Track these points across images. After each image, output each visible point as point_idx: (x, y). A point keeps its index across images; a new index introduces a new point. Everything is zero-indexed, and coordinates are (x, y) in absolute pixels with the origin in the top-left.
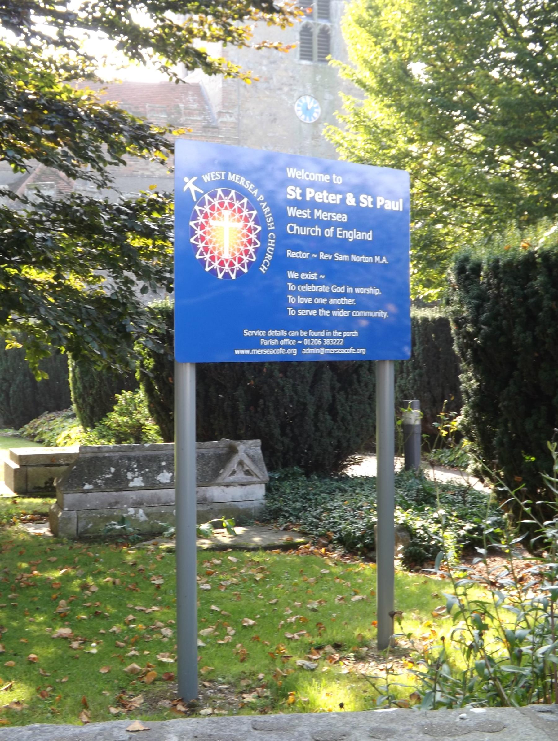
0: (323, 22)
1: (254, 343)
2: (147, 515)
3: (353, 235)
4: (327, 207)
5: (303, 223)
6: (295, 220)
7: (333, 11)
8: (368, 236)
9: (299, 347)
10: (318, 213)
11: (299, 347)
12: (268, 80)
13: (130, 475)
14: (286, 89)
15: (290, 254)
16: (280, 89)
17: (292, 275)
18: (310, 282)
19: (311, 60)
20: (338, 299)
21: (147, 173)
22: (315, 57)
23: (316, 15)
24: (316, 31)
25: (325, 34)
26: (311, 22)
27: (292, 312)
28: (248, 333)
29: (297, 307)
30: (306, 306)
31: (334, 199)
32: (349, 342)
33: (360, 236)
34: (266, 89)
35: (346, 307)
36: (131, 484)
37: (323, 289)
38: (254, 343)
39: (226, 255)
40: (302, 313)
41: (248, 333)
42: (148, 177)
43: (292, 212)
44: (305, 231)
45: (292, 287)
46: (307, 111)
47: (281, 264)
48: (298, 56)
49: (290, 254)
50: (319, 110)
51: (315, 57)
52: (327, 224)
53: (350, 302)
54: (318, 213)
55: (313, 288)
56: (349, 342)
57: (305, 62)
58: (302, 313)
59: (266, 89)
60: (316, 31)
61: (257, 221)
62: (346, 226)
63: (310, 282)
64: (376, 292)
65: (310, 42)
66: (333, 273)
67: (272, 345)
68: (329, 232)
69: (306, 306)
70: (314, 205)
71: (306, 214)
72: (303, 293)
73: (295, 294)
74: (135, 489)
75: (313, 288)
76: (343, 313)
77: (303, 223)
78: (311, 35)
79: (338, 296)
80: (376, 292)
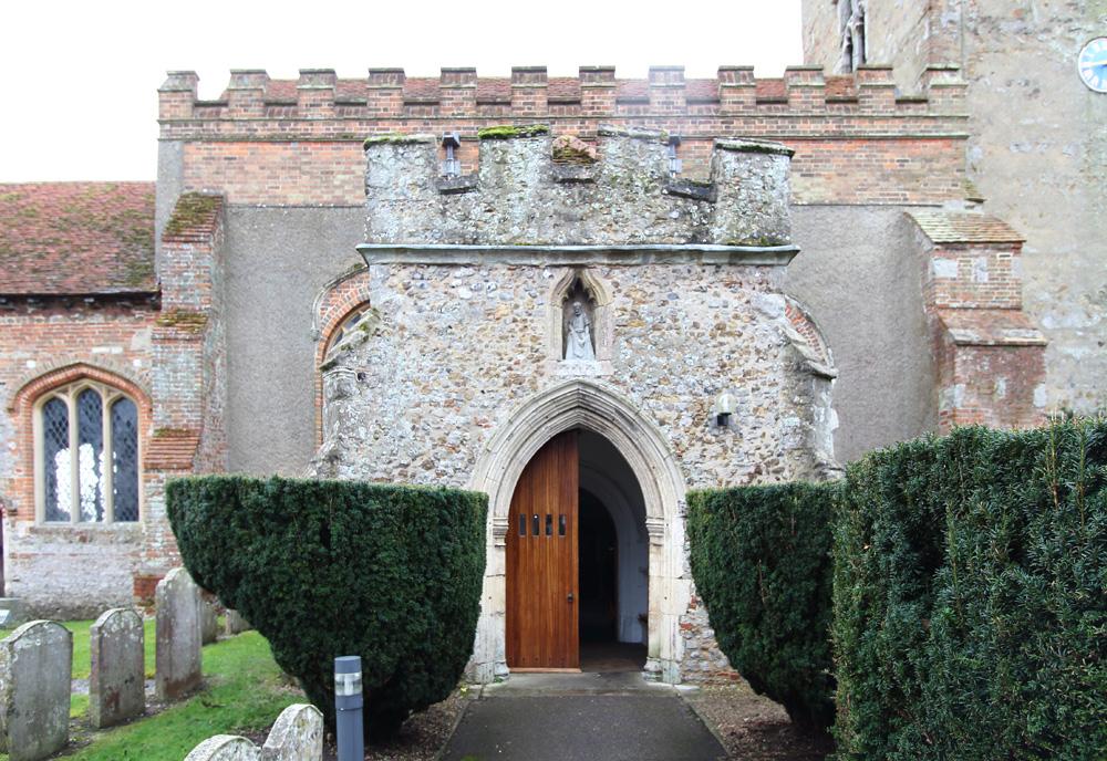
14: (1058, 30)
16: (1047, 30)
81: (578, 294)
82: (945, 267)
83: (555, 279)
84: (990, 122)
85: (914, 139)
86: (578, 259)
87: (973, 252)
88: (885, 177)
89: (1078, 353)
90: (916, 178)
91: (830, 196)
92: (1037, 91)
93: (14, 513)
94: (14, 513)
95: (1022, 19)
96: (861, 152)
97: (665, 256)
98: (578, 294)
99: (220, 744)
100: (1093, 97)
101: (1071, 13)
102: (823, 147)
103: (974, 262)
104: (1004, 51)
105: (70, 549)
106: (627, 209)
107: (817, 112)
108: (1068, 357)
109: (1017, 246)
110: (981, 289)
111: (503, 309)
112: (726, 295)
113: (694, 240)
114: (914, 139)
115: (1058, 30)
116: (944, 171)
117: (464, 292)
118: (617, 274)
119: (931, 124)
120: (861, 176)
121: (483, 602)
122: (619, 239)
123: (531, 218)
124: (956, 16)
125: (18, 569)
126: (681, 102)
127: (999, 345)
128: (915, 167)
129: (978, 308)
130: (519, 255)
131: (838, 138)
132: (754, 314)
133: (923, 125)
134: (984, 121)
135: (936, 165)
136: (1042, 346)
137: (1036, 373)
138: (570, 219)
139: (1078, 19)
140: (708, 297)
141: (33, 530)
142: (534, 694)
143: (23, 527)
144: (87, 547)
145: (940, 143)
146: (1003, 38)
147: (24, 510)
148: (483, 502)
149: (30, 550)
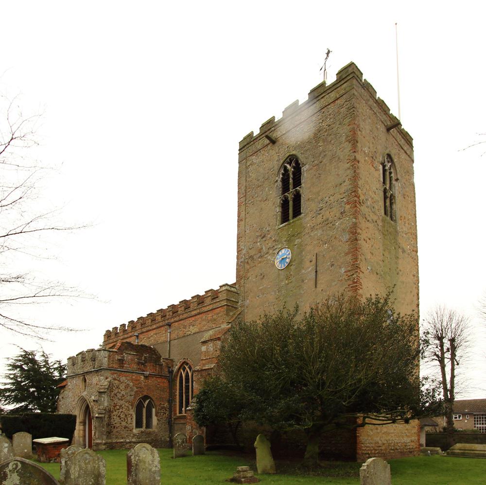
14: (271, 251)
84: (251, 292)
85: (214, 309)
87: (210, 343)
90: (215, 320)
91: (198, 330)
92: (264, 276)
95: (260, 252)
96: (204, 316)
99: (468, 343)
100: (280, 272)
102: (196, 317)
103: (209, 345)
104: (255, 266)
107: (195, 308)
114: (214, 309)
119: (218, 303)
120: (204, 323)
121: (76, 428)
126: (171, 314)
128: (215, 317)
129: (209, 358)
131: (199, 314)
133: (217, 304)
134: (249, 292)
135: (220, 315)
139: (276, 245)
145: (220, 309)
146: (255, 261)
148: (75, 417)
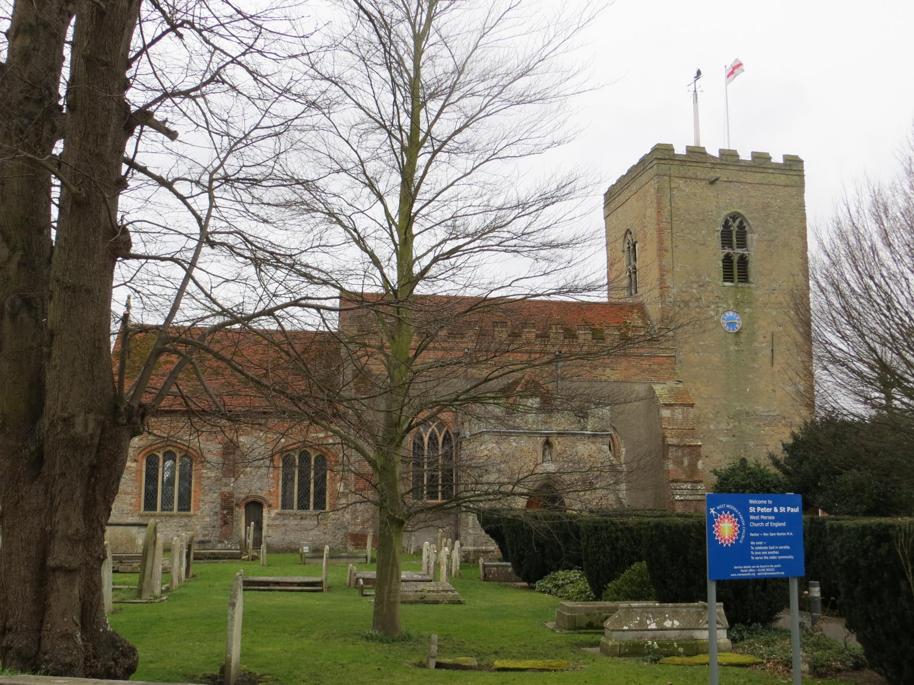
0: (740, 251)
1: (738, 571)
2: (659, 645)
3: (777, 525)
4: (766, 514)
5: (756, 521)
6: (753, 521)
7: (749, 242)
8: (784, 524)
9: (756, 572)
10: (762, 517)
11: (756, 572)
12: (698, 300)
13: (648, 622)
14: (713, 307)
15: (751, 534)
16: (708, 307)
17: (753, 543)
18: (759, 545)
19: (732, 282)
20: (773, 552)
21: (604, 378)
22: (736, 280)
23: (735, 246)
24: (736, 259)
25: (743, 261)
26: (731, 251)
27: (753, 558)
28: (736, 567)
29: (755, 556)
30: (758, 556)
31: (769, 510)
32: (777, 570)
33: (780, 524)
34: (697, 307)
35: (775, 555)
36: (650, 627)
37: (766, 548)
38: (738, 571)
39: (727, 537)
40: (757, 558)
41: (736, 567)
42: (605, 381)
43: (752, 517)
44: (757, 525)
45: (752, 548)
46: (731, 324)
47: (748, 539)
48: (722, 279)
49: (751, 534)
50: (741, 322)
51: (736, 280)
52: (765, 521)
53: (777, 553)
54: (762, 517)
55: (761, 548)
56: (777, 570)
57: (727, 284)
58: (757, 558)
59: (697, 307)
60: (736, 259)
61: (738, 523)
62: (774, 521)
63: (759, 545)
64: (788, 548)
65: (731, 267)
66: (770, 541)
67: (746, 572)
68: (767, 524)
69: (758, 556)
70: (760, 513)
71: (757, 518)
72: (759, 550)
73: (754, 551)
74: (652, 630)
75: (761, 548)
76: (774, 558)
77: (756, 521)
78: (732, 262)
79: (772, 550)
80: (788, 548)
81: (548, 444)
82: (666, 413)
83: (541, 440)
86: (548, 436)
88: (643, 371)
89: (725, 440)
90: (655, 371)
91: (622, 378)
93: (270, 506)
94: (270, 506)
97: (574, 435)
98: (548, 444)
101: (717, 300)
105: (295, 522)
106: (563, 420)
108: (721, 441)
109: (692, 405)
110: (679, 422)
111: (526, 449)
112: (592, 446)
113: (582, 430)
115: (713, 307)
116: (667, 369)
117: (514, 444)
118: (559, 439)
120: (634, 370)
122: (561, 428)
123: (534, 422)
124: (672, 300)
125: (270, 531)
127: (685, 446)
128: (655, 367)
130: (531, 434)
132: (600, 451)
136: (700, 446)
137: (699, 456)
138: (546, 423)
140: (586, 446)
141: (278, 514)
142: (632, 521)
143: (274, 513)
144: (303, 522)
147: (274, 505)
149: (277, 522)
